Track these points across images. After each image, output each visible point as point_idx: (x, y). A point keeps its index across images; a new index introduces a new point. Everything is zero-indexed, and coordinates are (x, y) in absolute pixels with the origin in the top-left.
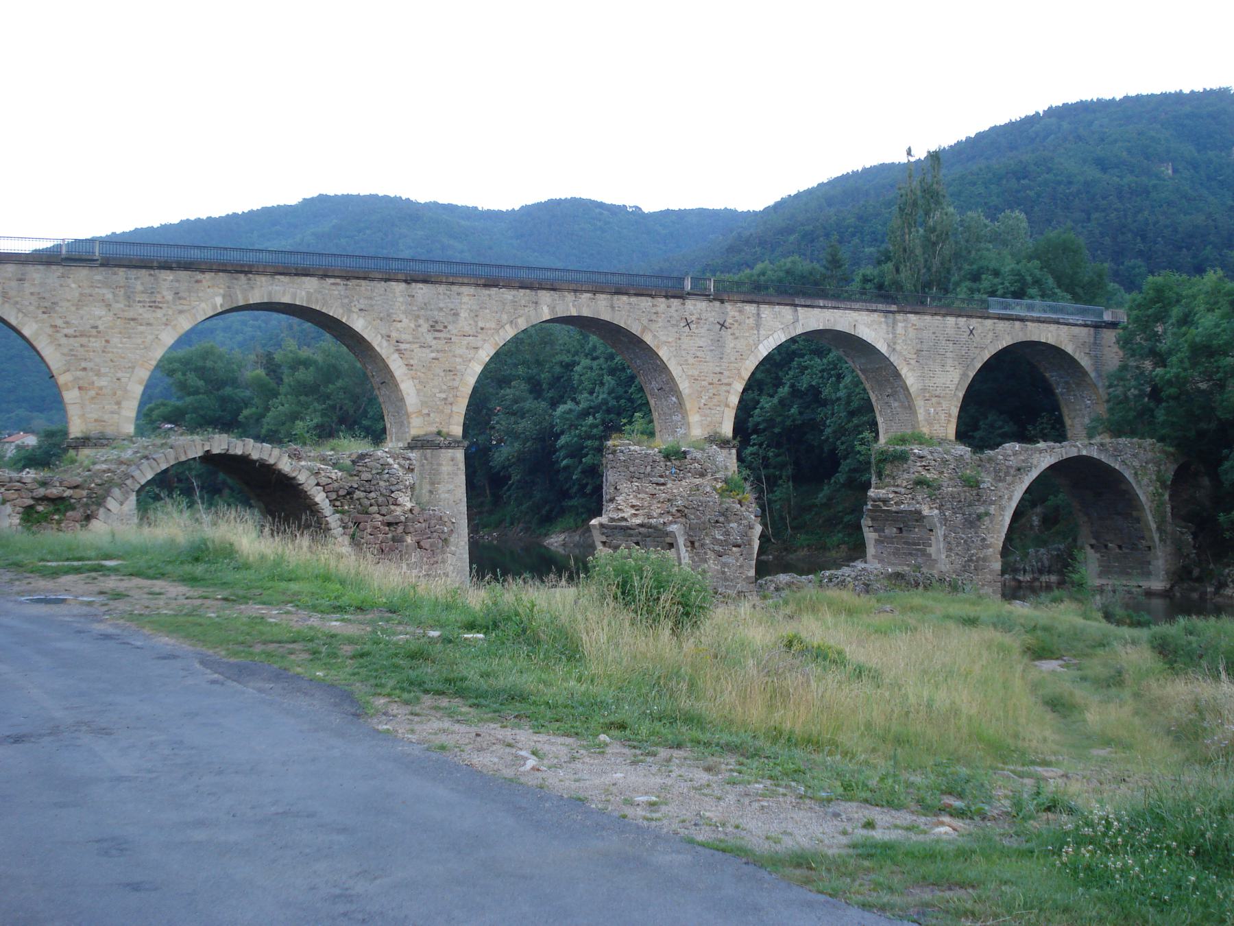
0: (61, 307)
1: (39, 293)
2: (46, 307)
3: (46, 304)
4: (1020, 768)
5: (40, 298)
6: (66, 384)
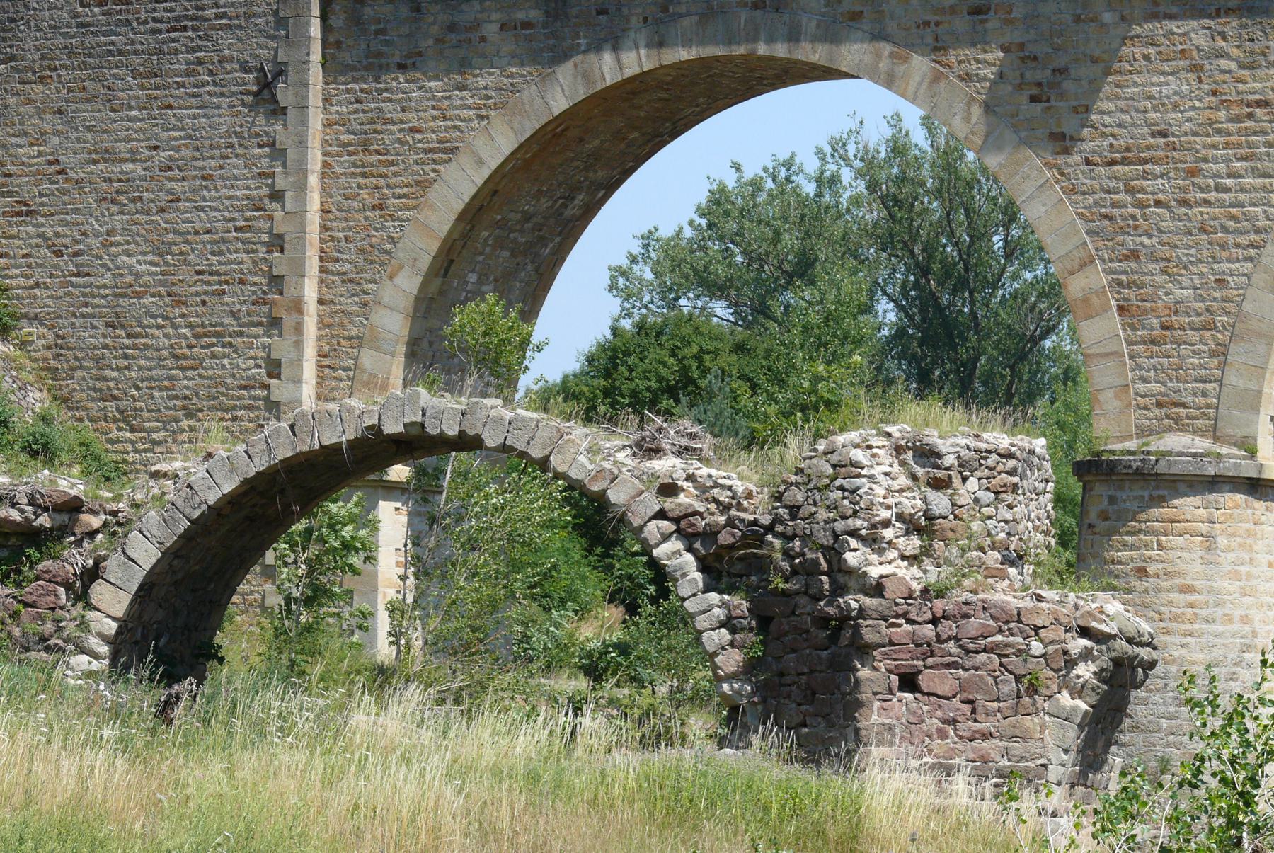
0: (1079, 80)
1: (1022, 46)
2: (1039, 85)
3: (1040, 75)
4: (1186, 251)
5: (1023, 59)
6: (1086, 300)
